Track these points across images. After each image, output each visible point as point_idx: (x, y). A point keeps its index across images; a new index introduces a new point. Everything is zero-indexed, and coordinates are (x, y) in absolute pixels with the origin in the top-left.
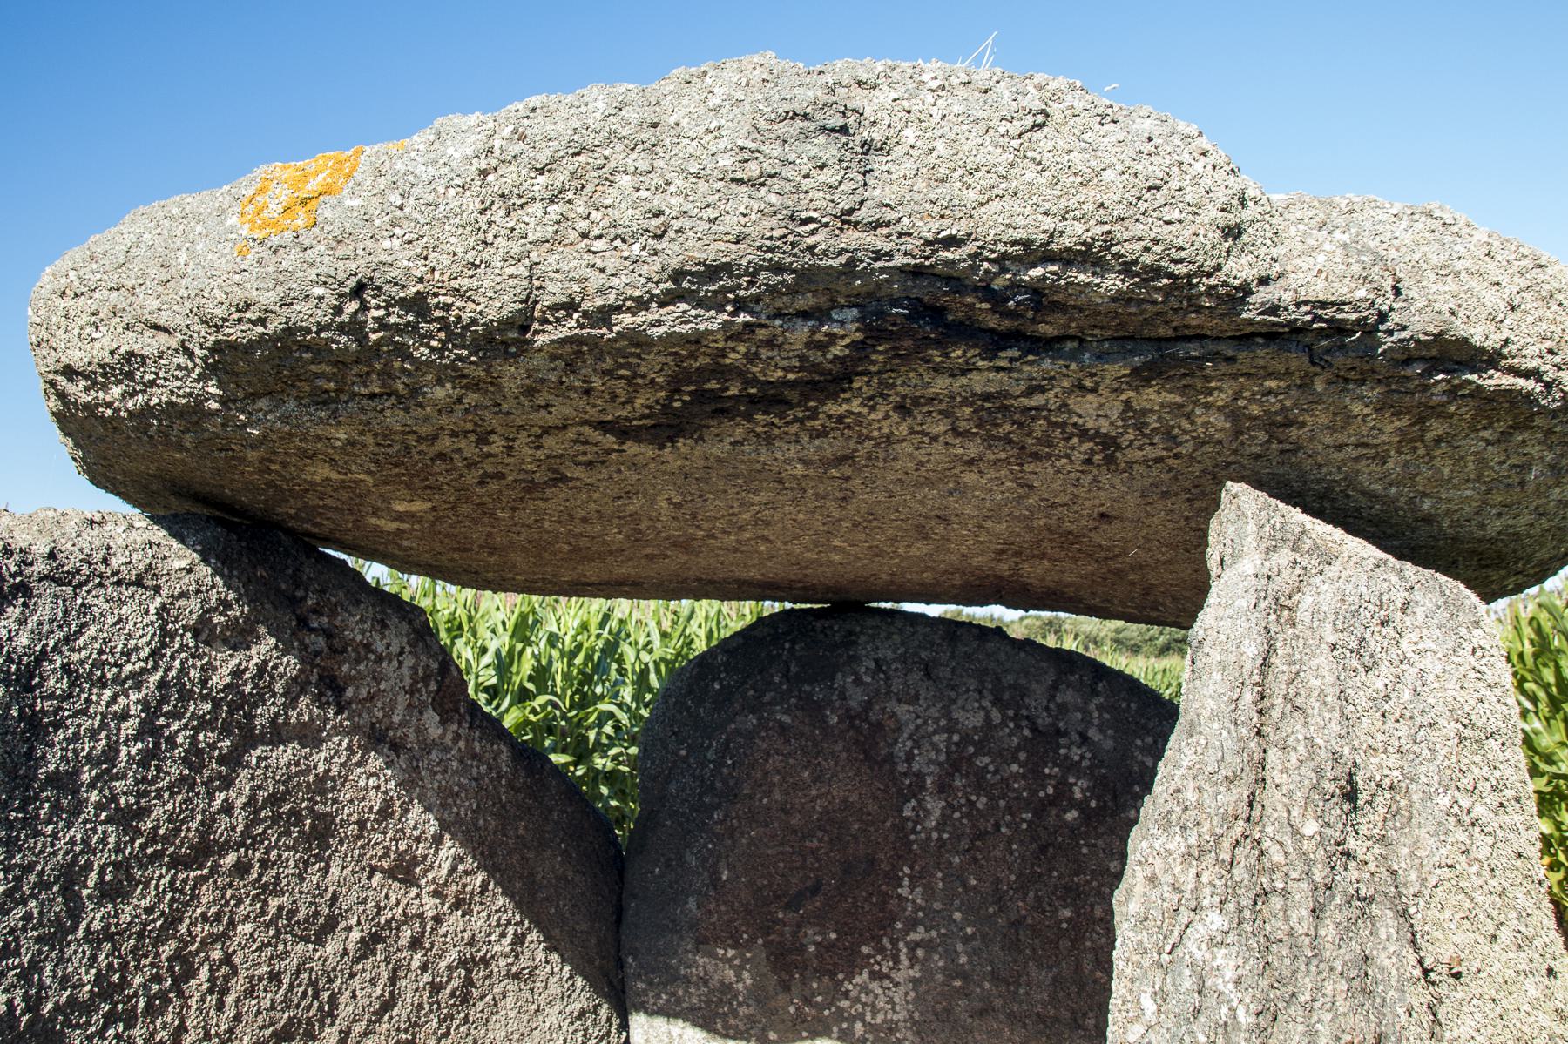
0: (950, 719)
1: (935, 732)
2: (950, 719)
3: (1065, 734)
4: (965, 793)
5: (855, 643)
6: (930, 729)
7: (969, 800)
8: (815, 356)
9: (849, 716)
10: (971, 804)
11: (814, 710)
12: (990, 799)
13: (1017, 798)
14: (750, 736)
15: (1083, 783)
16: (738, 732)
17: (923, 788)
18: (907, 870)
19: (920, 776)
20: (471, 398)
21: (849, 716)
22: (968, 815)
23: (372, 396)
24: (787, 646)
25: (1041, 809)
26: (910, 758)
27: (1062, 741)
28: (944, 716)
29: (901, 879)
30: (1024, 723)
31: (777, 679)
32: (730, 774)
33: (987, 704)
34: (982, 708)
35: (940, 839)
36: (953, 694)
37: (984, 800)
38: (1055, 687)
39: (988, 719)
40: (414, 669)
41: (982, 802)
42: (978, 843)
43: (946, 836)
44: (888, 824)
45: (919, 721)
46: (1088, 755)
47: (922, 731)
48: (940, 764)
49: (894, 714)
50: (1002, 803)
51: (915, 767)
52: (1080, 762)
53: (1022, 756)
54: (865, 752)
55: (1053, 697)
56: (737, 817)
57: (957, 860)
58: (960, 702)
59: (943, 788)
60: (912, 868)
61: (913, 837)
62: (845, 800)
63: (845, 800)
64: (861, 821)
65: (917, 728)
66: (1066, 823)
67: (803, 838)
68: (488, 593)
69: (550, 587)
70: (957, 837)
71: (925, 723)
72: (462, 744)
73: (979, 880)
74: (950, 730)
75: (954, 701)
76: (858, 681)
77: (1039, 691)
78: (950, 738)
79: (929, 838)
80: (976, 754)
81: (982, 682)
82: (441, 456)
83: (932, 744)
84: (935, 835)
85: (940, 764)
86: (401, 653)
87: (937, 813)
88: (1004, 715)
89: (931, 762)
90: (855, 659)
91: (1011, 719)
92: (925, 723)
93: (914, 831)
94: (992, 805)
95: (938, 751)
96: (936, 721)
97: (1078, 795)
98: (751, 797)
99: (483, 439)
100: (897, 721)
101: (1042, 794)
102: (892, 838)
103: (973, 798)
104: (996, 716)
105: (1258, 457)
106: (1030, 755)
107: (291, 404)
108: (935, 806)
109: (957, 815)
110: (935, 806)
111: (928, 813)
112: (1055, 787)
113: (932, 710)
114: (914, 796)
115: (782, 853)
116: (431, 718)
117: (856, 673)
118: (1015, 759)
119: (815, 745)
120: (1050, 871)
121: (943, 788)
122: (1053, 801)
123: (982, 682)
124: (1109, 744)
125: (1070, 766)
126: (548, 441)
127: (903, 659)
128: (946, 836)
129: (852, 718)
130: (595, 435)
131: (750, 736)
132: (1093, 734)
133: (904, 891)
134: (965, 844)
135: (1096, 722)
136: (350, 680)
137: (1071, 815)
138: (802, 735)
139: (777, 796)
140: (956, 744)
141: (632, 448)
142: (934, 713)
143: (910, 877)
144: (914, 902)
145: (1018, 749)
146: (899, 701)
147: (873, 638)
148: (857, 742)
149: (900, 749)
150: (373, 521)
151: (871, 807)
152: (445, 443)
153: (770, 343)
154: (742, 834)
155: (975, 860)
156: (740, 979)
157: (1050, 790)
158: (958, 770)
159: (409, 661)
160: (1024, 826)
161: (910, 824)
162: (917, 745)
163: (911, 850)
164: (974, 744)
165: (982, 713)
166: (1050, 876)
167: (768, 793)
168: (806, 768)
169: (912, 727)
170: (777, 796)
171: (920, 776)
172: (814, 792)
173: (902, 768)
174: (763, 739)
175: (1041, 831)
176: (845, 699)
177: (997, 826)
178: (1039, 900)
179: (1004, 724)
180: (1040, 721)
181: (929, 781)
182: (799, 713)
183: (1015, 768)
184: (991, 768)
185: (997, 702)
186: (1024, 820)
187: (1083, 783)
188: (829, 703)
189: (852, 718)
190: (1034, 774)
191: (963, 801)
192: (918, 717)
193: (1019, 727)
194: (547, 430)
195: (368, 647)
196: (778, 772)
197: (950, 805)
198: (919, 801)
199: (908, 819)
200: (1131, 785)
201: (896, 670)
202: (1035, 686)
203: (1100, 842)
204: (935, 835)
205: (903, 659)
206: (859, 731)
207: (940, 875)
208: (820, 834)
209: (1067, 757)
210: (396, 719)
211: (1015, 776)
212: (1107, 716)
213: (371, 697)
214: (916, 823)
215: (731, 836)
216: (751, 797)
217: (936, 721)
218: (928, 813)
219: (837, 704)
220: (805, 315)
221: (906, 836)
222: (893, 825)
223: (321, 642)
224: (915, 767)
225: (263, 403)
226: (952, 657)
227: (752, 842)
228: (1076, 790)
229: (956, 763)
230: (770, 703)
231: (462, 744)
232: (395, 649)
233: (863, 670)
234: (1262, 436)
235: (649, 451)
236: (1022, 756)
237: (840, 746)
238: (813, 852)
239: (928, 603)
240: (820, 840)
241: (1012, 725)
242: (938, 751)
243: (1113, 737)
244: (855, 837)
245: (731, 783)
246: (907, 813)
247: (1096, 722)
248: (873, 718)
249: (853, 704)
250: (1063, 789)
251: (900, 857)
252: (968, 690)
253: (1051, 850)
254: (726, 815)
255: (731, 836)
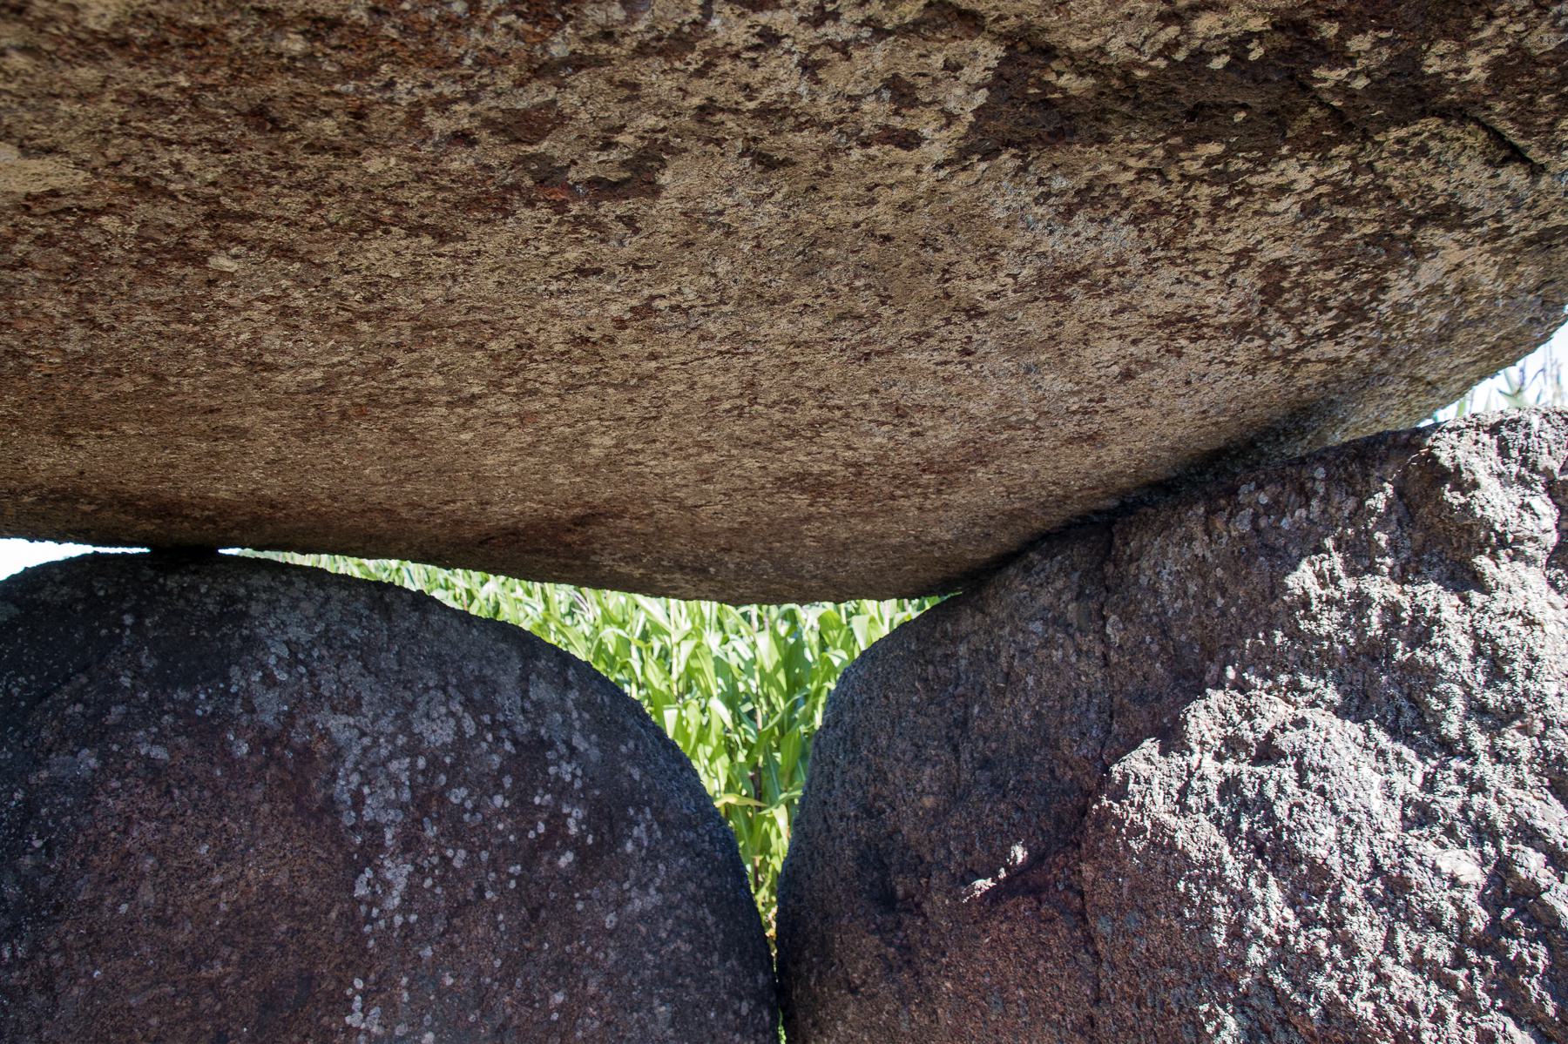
0: (411, 735)
1: (392, 756)
2: (411, 735)
3: (551, 745)
4: (439, 847)
5: (245, 615)
6: (384, 752)
7: (443, 858)
9: (265, 741)
10: (446, 861)
11: (208, 733)
12: (470, 852)
13: (503, 845)
14: (87, 790)
15: (578, 813)
16: (57, 785)
17: (381, 847)
18: (359, 984)
19: (375, 828)
21: (265, 741)
22: (442, 880)
24: (128, 620)
25: (532, 854)
26: (358, 801)
27: (550, 755)
28: (401, 730)
29: (350, 1000)
30: (504, 733)
31: (126, 682)
32: (43, 869)
33: (457, 708)
34: (451, 714)
35: (406, 924)
36: (408, 695)
37: (462, 853)
38: (524, 679)
39: (459, 731)
41: (459, 858)
42: (456, 921)
43: (413, 918)
44: (333, 915)
45: (366, 741)
46: (579, 772)
47: (372, 757)
48: (403, 807)
49: (326, 734)
50: (484, 855)
51: (368, 814)
52: (572, 783)
53: (507, 782)
54: (297, 800)
55: (525, 694)
56: (63, 948)
57: (428, 952)
58: (421, 707)
59: (410, 843)
60: (365, 979)
61: (368, 929)
62: (267, 885)
63: (267, 885)
64: (292, 916)
65: (365, 750)
66: (559, 871)
67: (196, 964)
68: (526, 626)
69: (42, 525)
70: (428, 917)
71: (375, 742)
73: (456, 977)
74: (413, 751)
75: (412, 706)
76: (269, 681)
77: (508, 681)
78: (413, 765)
79: (390, 927)
80: (449, 786)
81: (443, 675)
83: (389, 776)
84: (398, 920)
85: (403, 807)
87: (401, 884)
88: (479, 723)
89: (389, 804)
90: (251, 642)
91: (490, 728)
92: (375, 742)
93: (369, 920)
94: (472, 862)
95: (398, 786)
96: (391, 739)
97: (573, 830)
98: (93, 906)
100: (333, 741)
101: (532, 835)
102: (339, 936)
103: (450, 853)
104: (469, 726)
106: (516, 780)
108: (398, 873)
109: (428, 882)
110: (398, 873)
111: (388, 885)
112: (547, 823)
113: (384, 722)
114: (369, 862)
115: (157, 999)
117: (263, 666)
118: (499, 787)
119: (217, 795)
120: (541, 943)
121: (410, 843)
122: (545, 843)
123: (443, 675)
124: (595, 754)
125: (562, 790)
127: (327, 639)
128: (413, 918)
129: (269, 743)
131: (87, 790)
132: (577, 740)
133: (353, 1020)
134: (439, 926)
135: (577, 725)
137: (566, 859)
138: (192, 779)
139: (147, 894)
140: (423, 772)
142: (386, 725)
143: (364, 994)
144: (368, 1032)
145: (502, 771)
146: (334, 710)
147: (272, 605)
148: (282, 784)
149: (343, 788)
151: (307, 890)
154: (73, 979)
155: (453, 946)
157: (541, 828)
158: (427, 814)
160: (513, 884)
161: (363, 908)
162: (367, 780)
163: (365, 950)
164: (446, 770)
165: (452, 722)
166: (540, 951)
167: (131, 894)
168: (204, 838)
169: (357, 750)
171: (375, 828)
172: (217, 880)
173: (349, 819)
174: (114, 794)
175: (532, 888)
176: (253, 711)
177: (480, 891)
178: (527, 987)
179: (480, 736)
180: (518, 728)
181: (389, 836)
182: (182, 741)
183: (499, 800)
184: (469, 804)
185: (468, 703)
186: (511, 876)
187: (578, 813)
188: (229, 721)
189: (269, 743)
190: (522, 807)
191: (435, 860)
192: (363, 734)
193: (498, 739)
196: (151, 852)
197: (419, 869)
198: (377, 870)
199: (360, 901)
200: (625, 808)
201: (321, 658)
202: (503, 679)
203: (595, 892)
204: (398, 920)
205: (327, 639)
206: (281, 762)
207: (405, 980)
208: (226, 951)
209: (558, 778)
211: (500, 814)
212: (586, 716)
214: (371, 905)
215: (48, 988)
216: (93, 906)
217: (391, 739)
218: (388, 885)
219: (244, 721)
221: (358, 928)
222: (341, 914)
224: (368, 814)
226: (392, 638)
227: (94, 990)
228: (571, 822)
229: (425, 802)
230: (119, 726)
233: (272, 661)
236: (507, 782)
237: (257, 794)
238: (213, 985)
239: (304, 553)
240: (226, 963)
241: (490, 737)
242: (398, 786)
243: (598, 745)
244: (281, 946)
245: (44, 883)
246: (361, 891)
247: (577, 725)
248: (298, 740)
249: (268, 719)
250: (557, 820)
251: (349, 964)
252: (427, 689)
253: (543, 914)
254: (35, 948)
255: (48, 988)
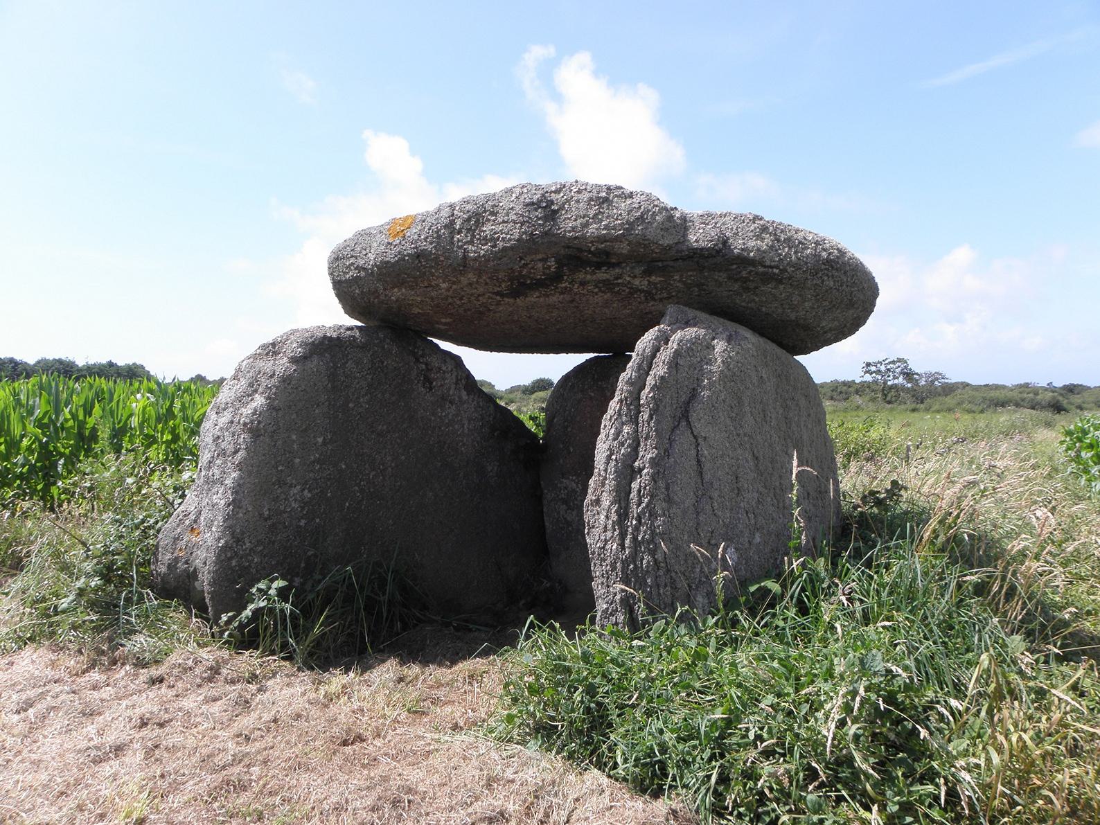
8: (548, 272)
20: (454, 287)
23: (426, 287)
40: (457, 376)
72: (475, 402)
82: (450, 304)
86: (452, 370)
99: (461, 299)
105: (699, 296)
107: (404, 290)
116: (464, 393)
126: (481, 298)
130: (494, 296)
136: (436, 380)
139: (589, 421)
141: (506, 300)
150: (437, 326)
152: (450, 300)
153: (533, 268)
156: (578, 487)
159: (455, 374)
170: (589, 421)
194: (479, 295)
195: (440, 368)
210: (451, 393)
213: (442, 385)
220: (540, 260)
223: (424, 366)
225: (396, 290)
231: (475, 402)
232: (449, 369)
234: (696, 289)
235: (511, 300)
